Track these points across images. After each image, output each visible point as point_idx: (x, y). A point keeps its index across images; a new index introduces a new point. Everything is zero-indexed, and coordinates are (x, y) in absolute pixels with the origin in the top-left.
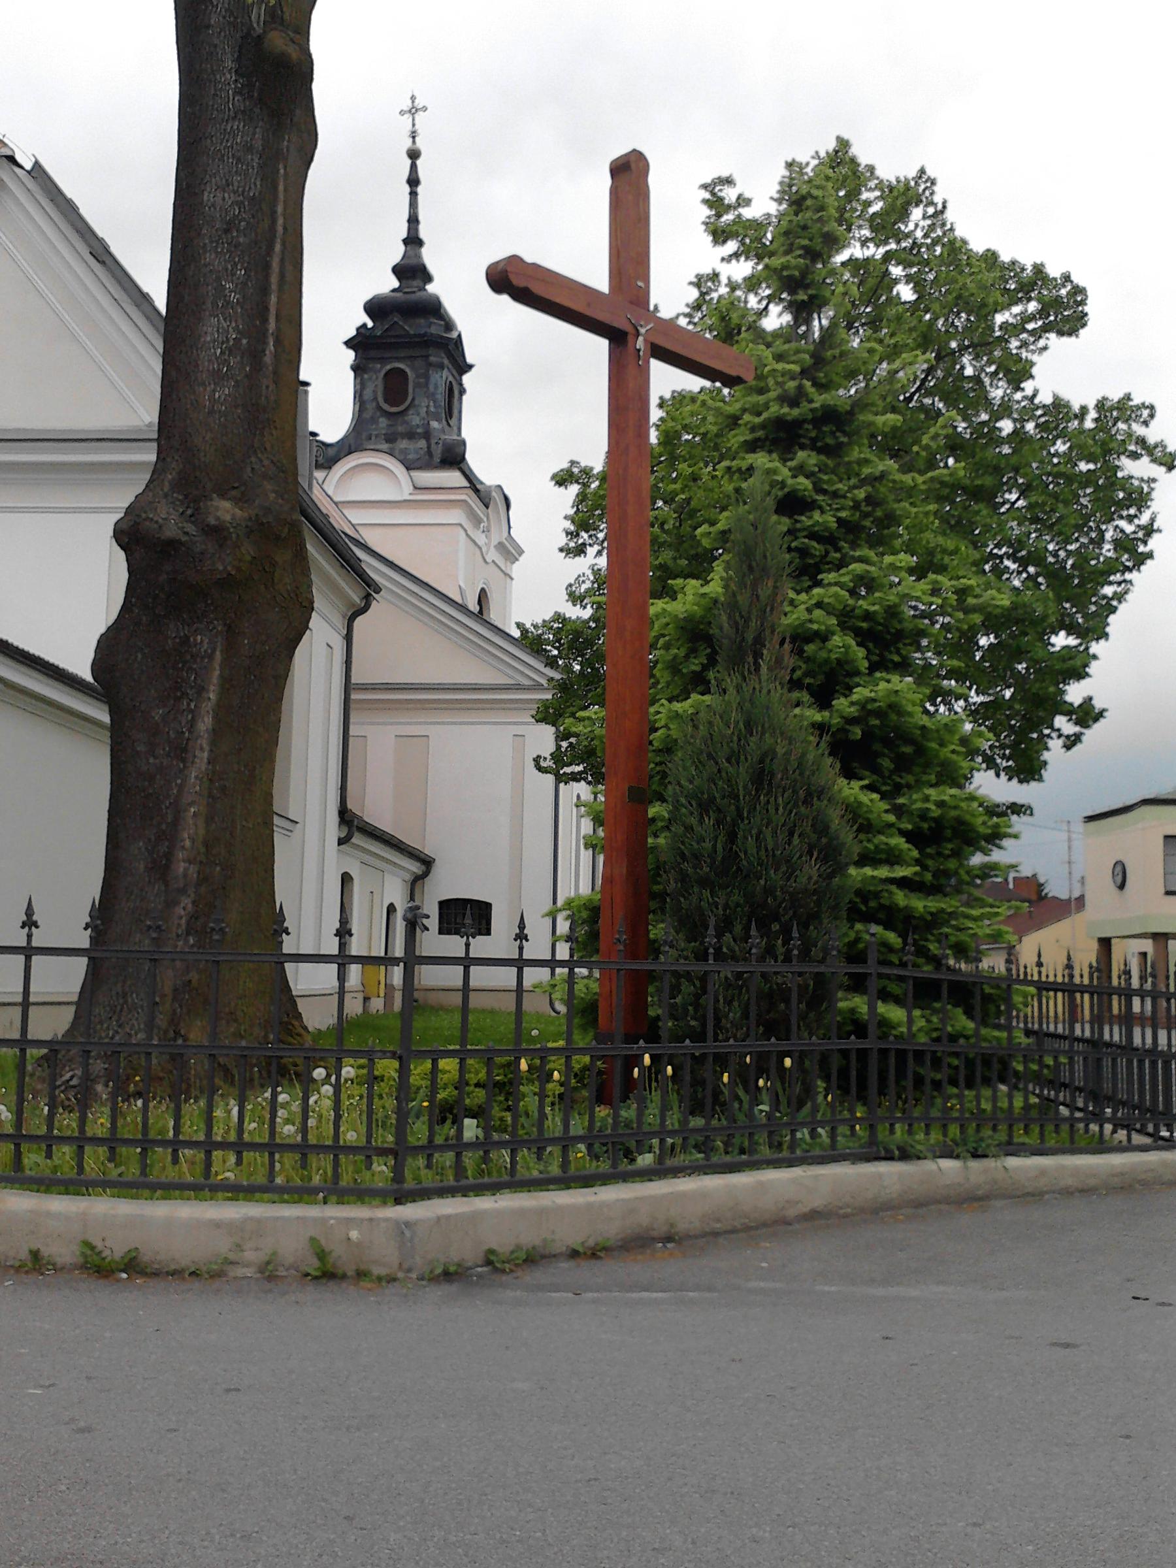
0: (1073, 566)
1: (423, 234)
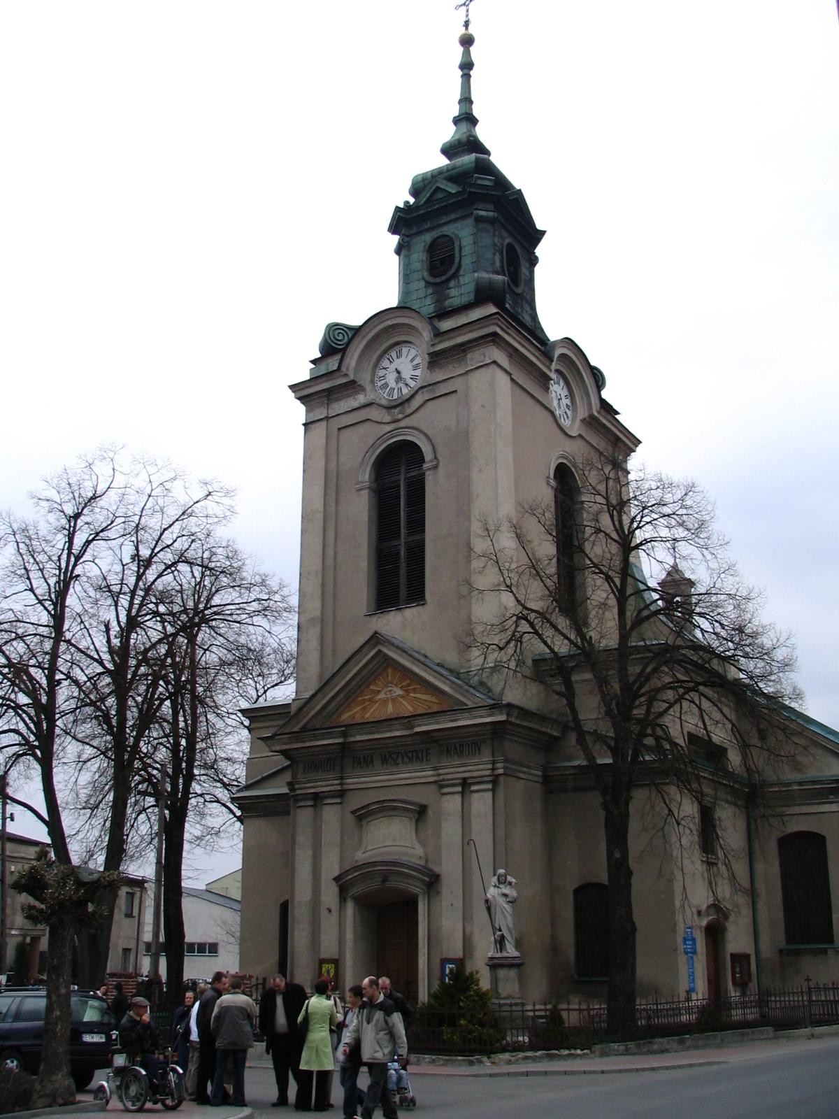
0: (678, 601)
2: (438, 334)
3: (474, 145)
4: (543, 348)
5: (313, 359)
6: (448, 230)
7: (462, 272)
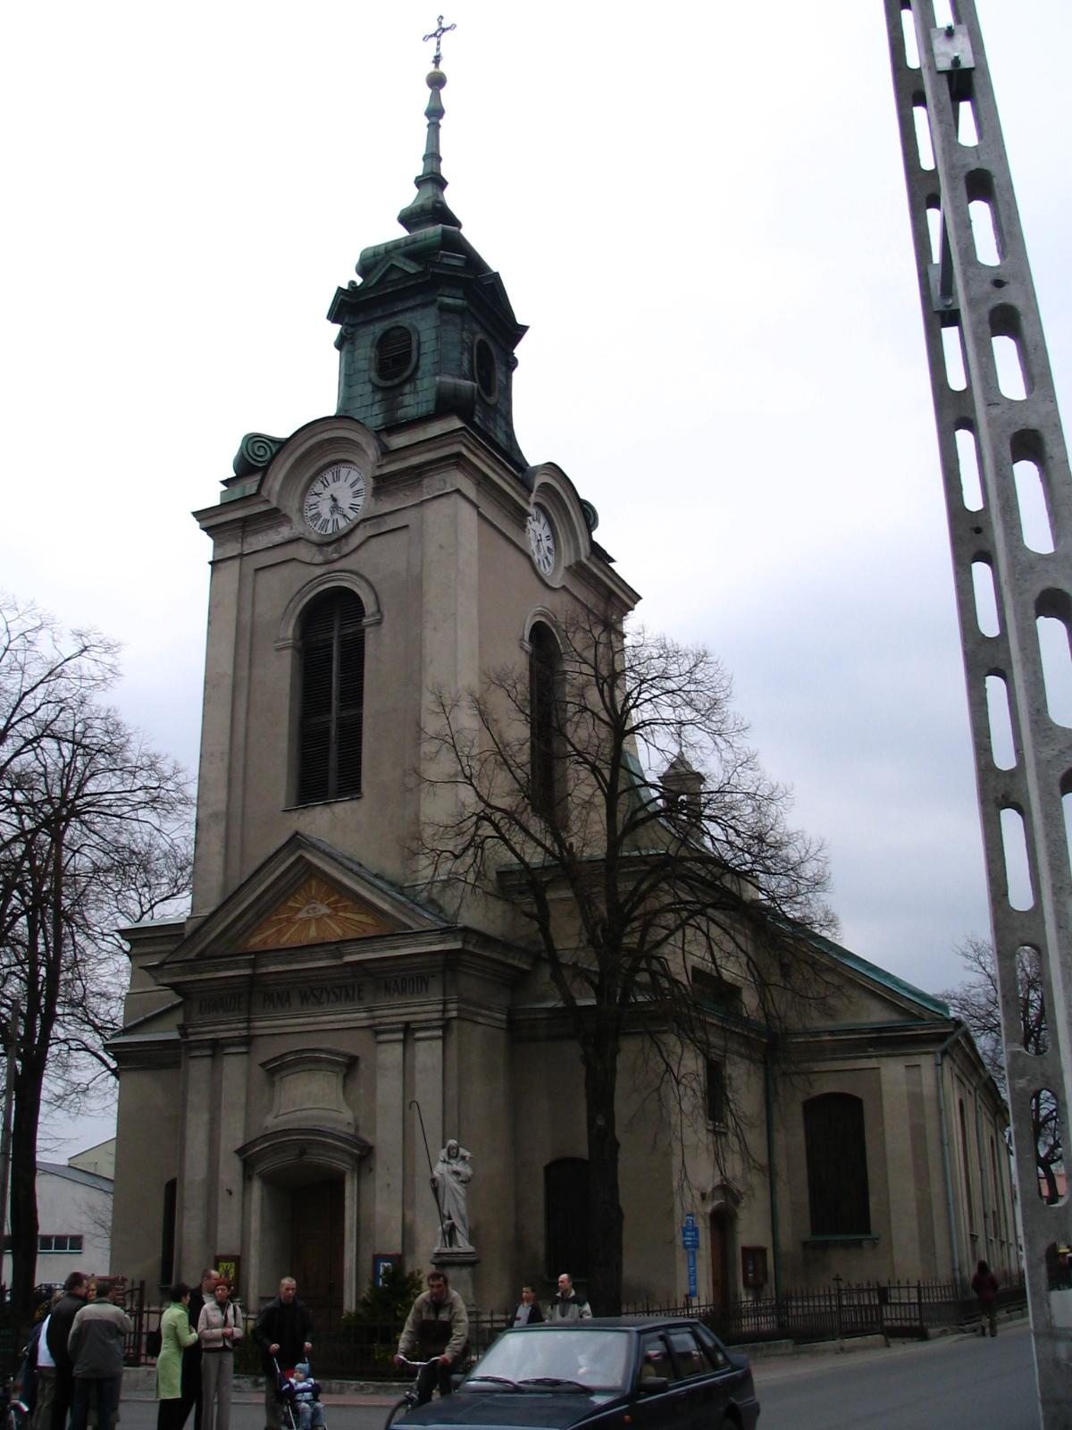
1: (446, 171)
2: (386, 453)
3: (441, 214)
4: (520, 475)
5: (225, 478)
6: (404, 320)
7: (419, 374)
